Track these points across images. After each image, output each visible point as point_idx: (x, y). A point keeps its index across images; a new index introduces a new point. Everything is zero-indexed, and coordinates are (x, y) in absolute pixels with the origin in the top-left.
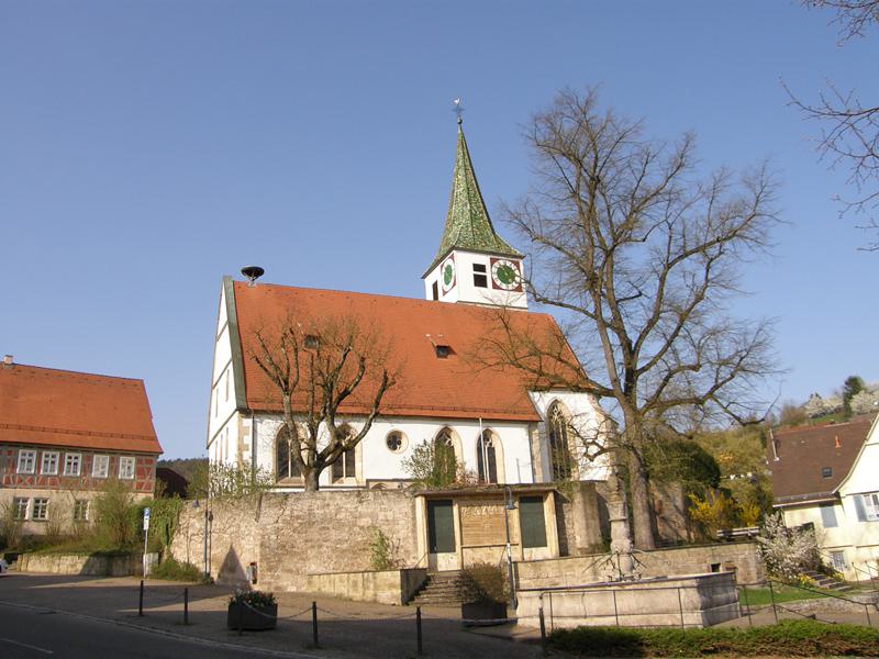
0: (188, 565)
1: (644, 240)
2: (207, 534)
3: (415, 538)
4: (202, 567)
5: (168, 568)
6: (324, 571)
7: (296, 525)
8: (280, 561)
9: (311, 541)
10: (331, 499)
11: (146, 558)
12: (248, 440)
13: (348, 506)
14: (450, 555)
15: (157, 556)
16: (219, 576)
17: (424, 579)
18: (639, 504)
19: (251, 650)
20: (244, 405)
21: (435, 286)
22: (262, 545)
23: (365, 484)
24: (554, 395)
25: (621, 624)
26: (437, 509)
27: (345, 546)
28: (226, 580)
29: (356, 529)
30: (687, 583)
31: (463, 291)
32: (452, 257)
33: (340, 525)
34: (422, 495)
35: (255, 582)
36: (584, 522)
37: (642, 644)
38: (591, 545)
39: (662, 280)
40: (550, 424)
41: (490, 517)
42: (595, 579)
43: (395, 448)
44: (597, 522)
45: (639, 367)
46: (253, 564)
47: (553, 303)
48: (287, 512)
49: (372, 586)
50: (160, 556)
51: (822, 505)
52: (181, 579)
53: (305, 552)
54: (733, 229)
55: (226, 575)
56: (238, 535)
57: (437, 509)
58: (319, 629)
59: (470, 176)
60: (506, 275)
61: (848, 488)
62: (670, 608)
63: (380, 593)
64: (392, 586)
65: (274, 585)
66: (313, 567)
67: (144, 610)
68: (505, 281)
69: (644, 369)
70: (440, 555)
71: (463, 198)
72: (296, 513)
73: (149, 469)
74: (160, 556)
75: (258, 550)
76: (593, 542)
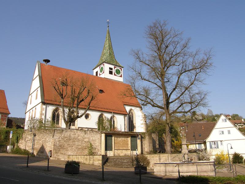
0: (25, 150)
1: (179, 66)
2: (34, 140)
3: (101, 146)
4: (31, 151)
5: (18, 151)
6: (73, 154)
7: (65, 140)
8: (59, 150)
9: (69, 145)
10: (76, 132)
11: (8, 147)
12: (44, 112)
13: (82, 135)
14: (111, 151)
15: (13, 146)
16: (37, 154)
17: (107, 158)
18: (168, 140)
19: (84, 181)
20: (43, 101)
21: (97, 73)
22: (54, 145)
23: (78, 129)
24: (131, 107)
25: (199, 175)
26: (108, 138)
27: (80, 147)
28: (39, 155)
29: (84, 142)
30: (211, 163)
31: (106, 75)
32: (104, 65)
33: (79, 140)
34: (104, 133)
35: (51, 157)
36: (149, 144)
37: (208, 181)
38: (150, 151)
39: (179, 78)
40: (129, 116)
41: (123, 141)
42: (160, 162)
43: (87, 119)
44: (152, 144)
45: (170, 101)
46: (51, 151)
47: (147, 80)
48: (63, 135)
49: (92, 160)
50: (14, 147)
51: (198, 144)
52: (23, 154)
53: (67, 148)
54: (202, 66)
55: (40, 154)
56: (45, 141)
57: (108, 138)
58: (104, 176)
59: (110, 42)
60: (118, 72)
61: (208, 140)
62: (206, 171)
63: (94, 162)
64: (99, 160)
65: (57, 158)
66: (70, 153)
67: (28, 165)
68: (118, 73)
69: (172, 102)
70: (108, 151)
71: (107, 48)
72: (65, 136)
73: (5, 119)
74: (14, 147)
75: (53, 147)
76: (151, 150)
